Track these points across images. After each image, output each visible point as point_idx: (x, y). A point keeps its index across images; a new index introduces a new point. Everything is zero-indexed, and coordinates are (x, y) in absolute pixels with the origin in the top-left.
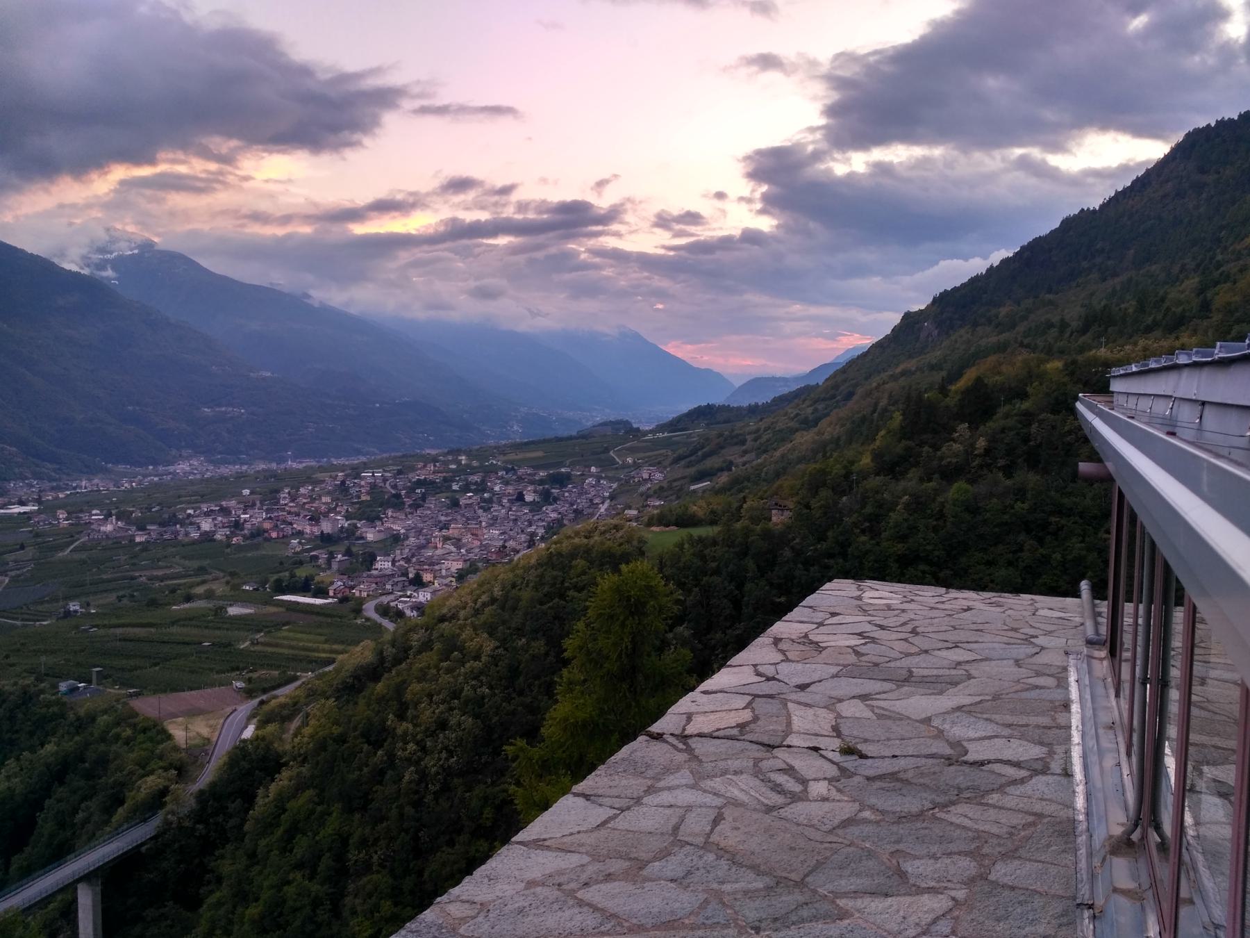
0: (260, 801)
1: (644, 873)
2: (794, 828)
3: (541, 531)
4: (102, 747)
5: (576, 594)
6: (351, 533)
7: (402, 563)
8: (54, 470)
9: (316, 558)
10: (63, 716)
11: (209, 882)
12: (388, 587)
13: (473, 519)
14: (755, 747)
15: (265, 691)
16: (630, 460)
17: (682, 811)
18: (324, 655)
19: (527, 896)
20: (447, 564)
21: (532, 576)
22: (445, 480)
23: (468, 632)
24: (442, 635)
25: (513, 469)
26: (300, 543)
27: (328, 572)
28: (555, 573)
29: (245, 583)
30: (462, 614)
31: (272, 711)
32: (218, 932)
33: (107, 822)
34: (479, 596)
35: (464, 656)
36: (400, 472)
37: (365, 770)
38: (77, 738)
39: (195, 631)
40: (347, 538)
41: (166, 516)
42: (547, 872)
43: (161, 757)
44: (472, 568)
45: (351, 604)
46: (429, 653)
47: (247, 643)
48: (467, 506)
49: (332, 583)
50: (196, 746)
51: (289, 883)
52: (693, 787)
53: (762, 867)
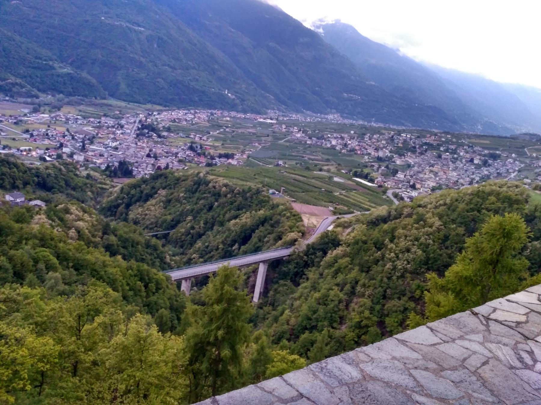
0: (329, 255)
1: (442, 373)
2: (519, 381)
3: (477, 179)
4: (279, 217)
5: (486, 212)
6: (390, 159)
7: (409, 177)
8: (285, 109)
9: (373, 166)
10: (268, 202)
11: (304, 279)
12: (400, 186)
13: (446, 165)
14: (520, 335)
15: (340, 214)
16: (534, 155)
17: (471, 353)
18: (366, 207)
19: (390, 362)
20: (429, 182)
21: (467, 198)
22: (438, 145)
23: (430, 215)
24: (418, 213)
25: (472, 146)
26: (368, 158)
27: (377, 173)
28: (478, 200)
29: (343, 169)
30: (429, 206)
31: (341, 223)
32: (303, 298)
33: (275, 244)
34: (439, 201)
35: (425, 224)
36: (418, 137)
37: (372, 257)
38: (271, 211)
39: (320, 184)
40: (388, 161)
41: (320, 135)
42: (402, 356)
43: (297, 227)
44: (440, 188)
45: (383, 189)
46: (410, 219)
47: (338, 193)
48: (445, 159)
49: (377, 178)
50: (311, 227)
51: (332, 290)
52: (482, 344)
53: (495, 393)
